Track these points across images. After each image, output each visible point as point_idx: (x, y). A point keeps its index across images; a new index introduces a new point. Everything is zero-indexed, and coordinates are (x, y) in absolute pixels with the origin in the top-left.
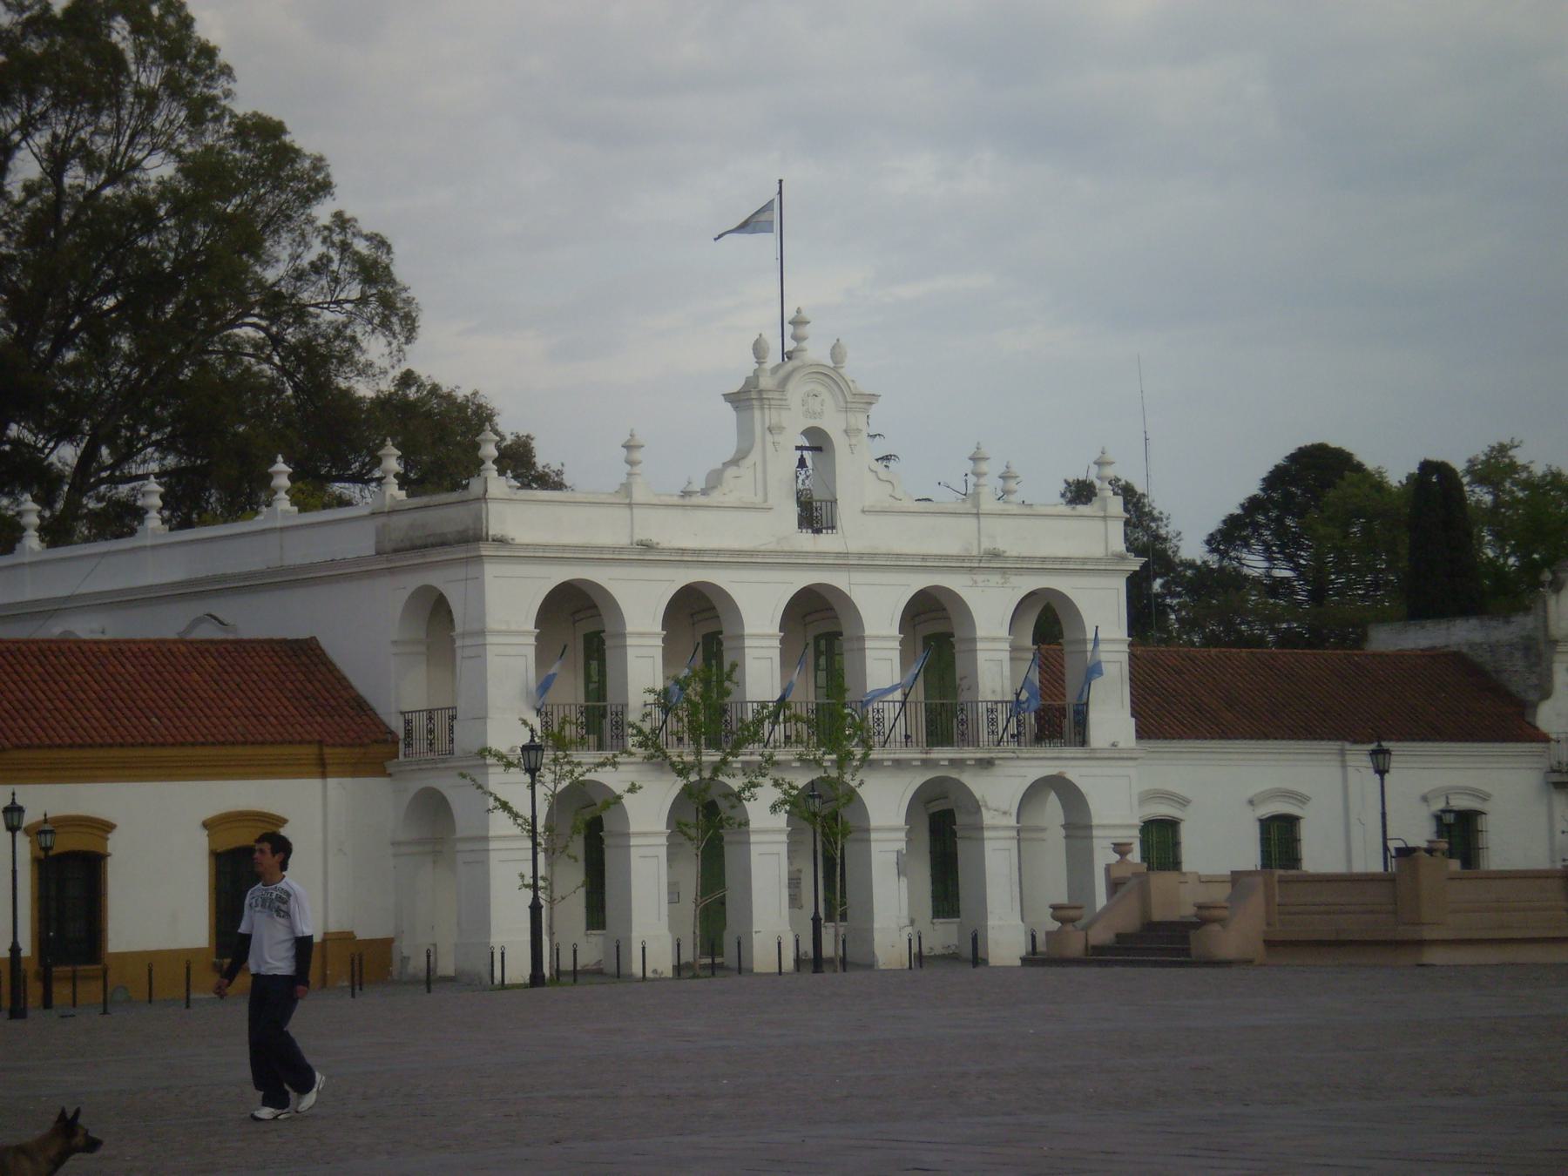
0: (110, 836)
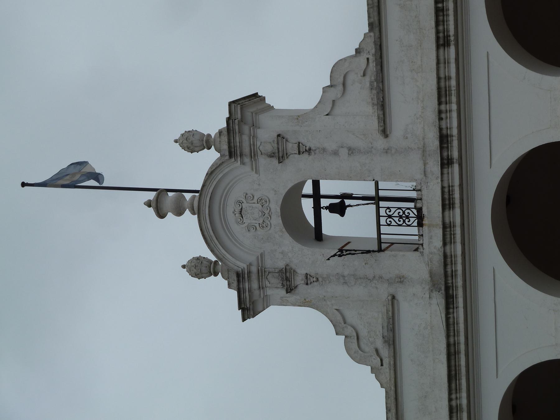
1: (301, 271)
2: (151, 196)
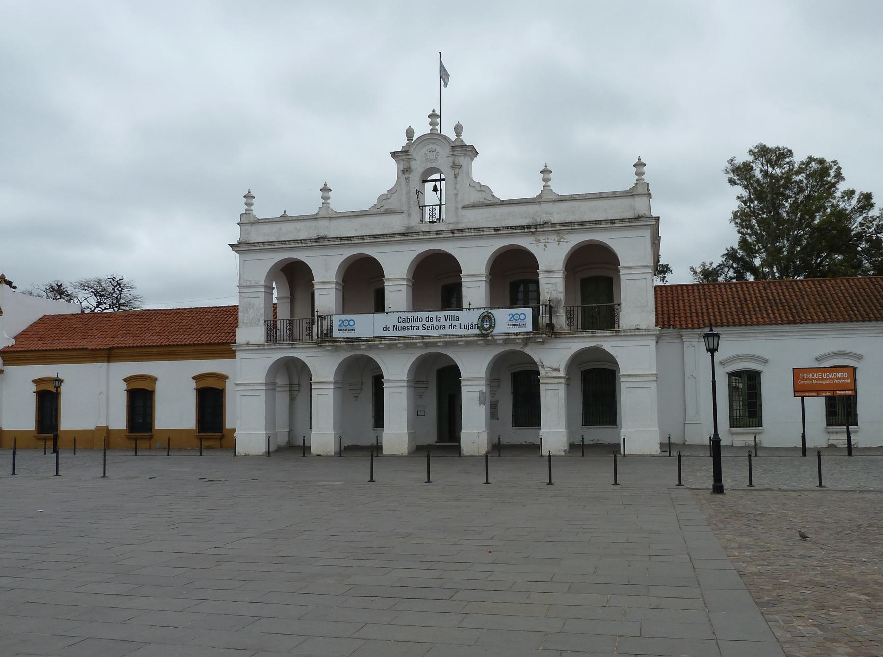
0: (156, 382)
1: (410, 176)
2: (437, 112)
